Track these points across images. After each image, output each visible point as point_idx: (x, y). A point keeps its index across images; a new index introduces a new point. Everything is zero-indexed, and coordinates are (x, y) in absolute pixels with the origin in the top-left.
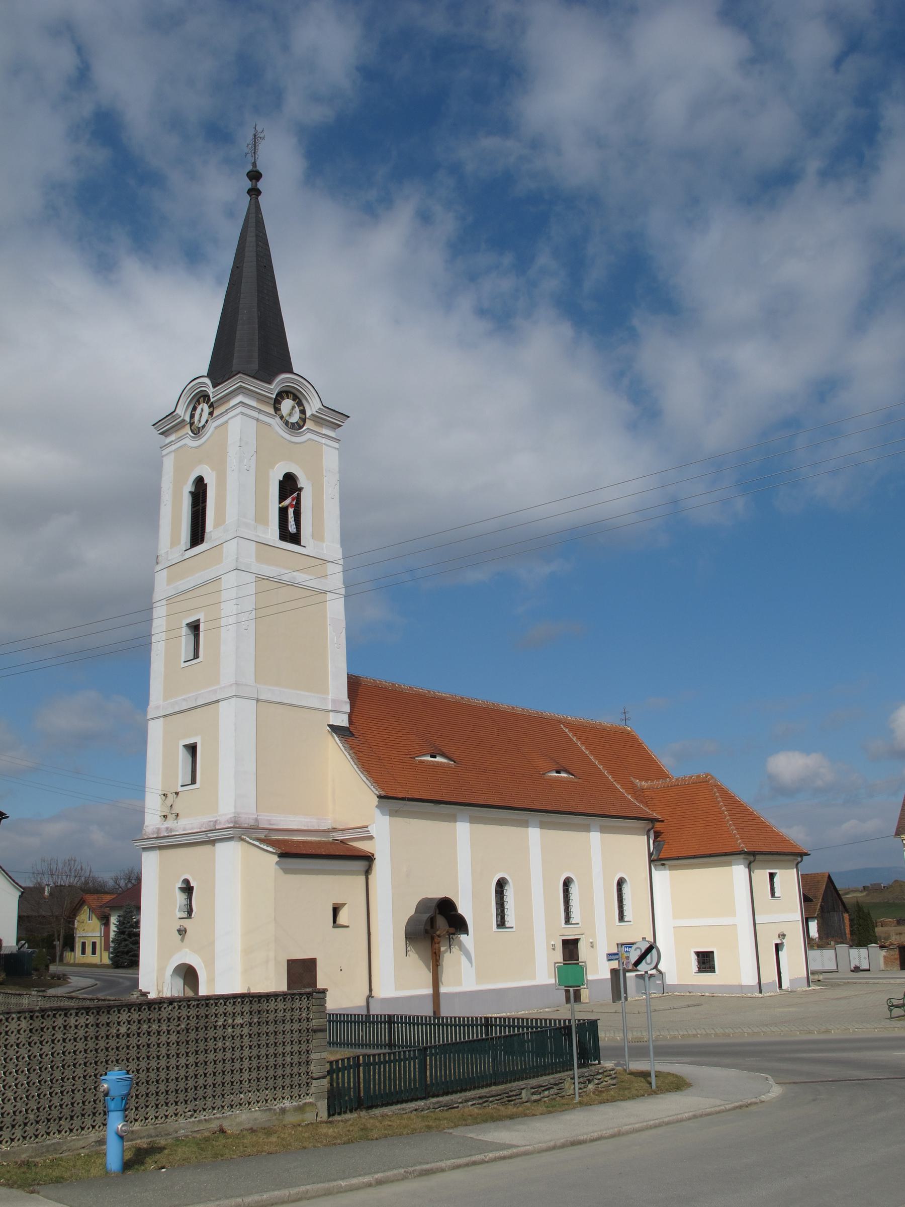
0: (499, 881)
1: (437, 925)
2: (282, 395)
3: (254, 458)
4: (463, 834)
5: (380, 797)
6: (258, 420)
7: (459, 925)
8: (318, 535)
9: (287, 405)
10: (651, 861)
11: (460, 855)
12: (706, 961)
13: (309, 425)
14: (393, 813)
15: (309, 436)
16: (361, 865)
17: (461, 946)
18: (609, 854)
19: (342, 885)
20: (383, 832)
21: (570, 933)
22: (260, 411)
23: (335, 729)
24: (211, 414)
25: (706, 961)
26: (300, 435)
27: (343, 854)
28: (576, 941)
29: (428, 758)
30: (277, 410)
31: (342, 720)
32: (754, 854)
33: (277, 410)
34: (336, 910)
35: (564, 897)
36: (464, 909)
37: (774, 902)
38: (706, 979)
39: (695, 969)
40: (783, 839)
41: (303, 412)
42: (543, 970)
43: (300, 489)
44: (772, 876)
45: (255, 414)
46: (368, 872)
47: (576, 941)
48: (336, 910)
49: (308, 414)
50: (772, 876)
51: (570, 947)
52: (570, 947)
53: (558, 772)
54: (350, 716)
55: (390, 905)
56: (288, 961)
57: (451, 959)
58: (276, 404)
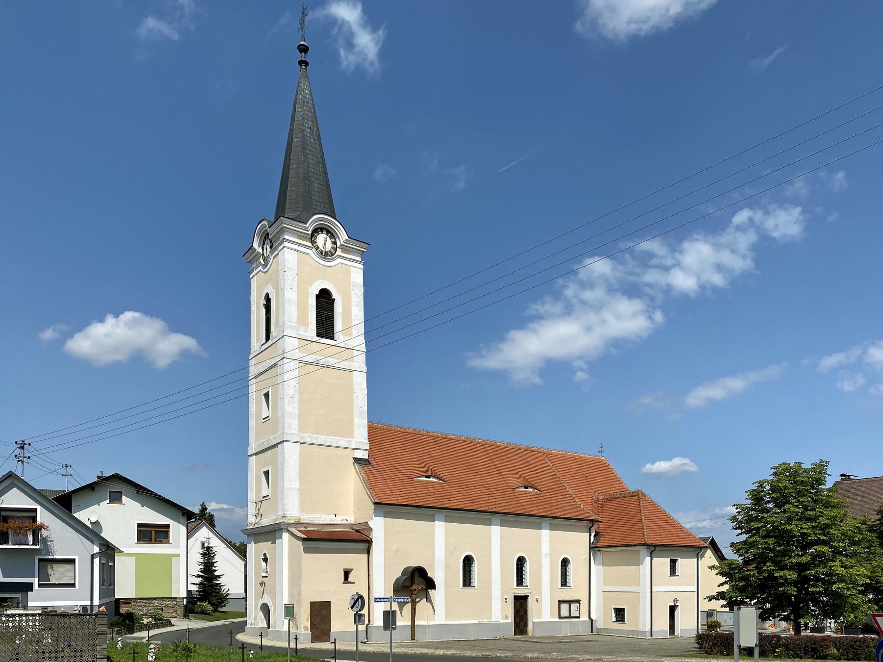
0: (464, 560)
1: (415, 583)
2: (316, 231)
3: (296, 279)
4: (440, 529)
5: (375, 503)
6: (298, 251)
7: (431, 584)
8: (347, 329)
9: (321, 238)
10: (590, 548)
11: (437, 544)
12: (620, 614)
13: (339, 252)
14: (386, 515)
15: (339, 260)
16: (364, 546)
17: (429, 600)
18: (549, 546)
19: (355, 561)
20: (379, 526)
21: (521, 591)
22: (299, 244)
23: (357, 460)
24: (271, 247)
25: (620, 614)
26: (330, 260)
27: (357, 539)
28: (526, 598)
29: (424, 479)
30: (313, 242)
31: (363, 455)
32: (655, 546)
33: (313, 242)
34: (347, 573)
35: (517, 572)
36: (437, 574)
37: (674, 578)
38: (619, 626)
39: (614, 619)
40: (687, 534)
41: (335, 243)
42: (502, 614)
43: (334, 300)
44: (673, 562)
45: (296, 247)
46: (368, 552)
47: (526, 598)
48: (347, 573)
49: (339, 244)
50: (673, 562)
51: (521, 604)
52: (521, 604)
53: (526, 487)
54: (370, 451)
55: (381, 573)
56: (328, 604)
57: (422, 604)
58: (312, 237)
